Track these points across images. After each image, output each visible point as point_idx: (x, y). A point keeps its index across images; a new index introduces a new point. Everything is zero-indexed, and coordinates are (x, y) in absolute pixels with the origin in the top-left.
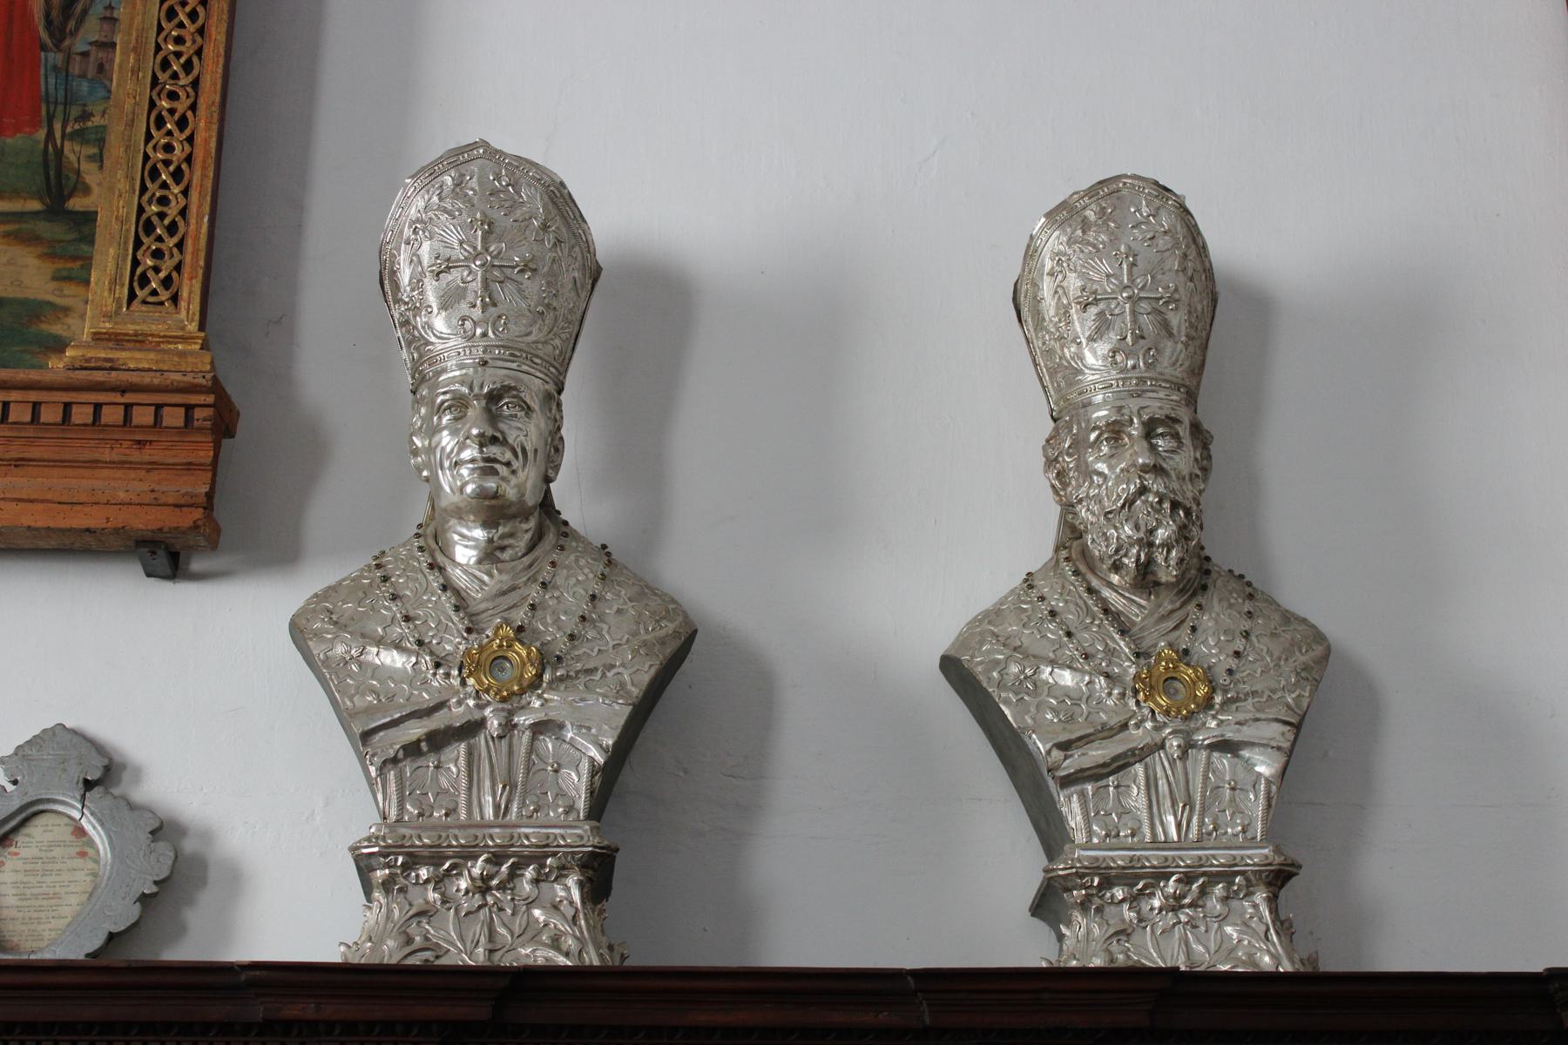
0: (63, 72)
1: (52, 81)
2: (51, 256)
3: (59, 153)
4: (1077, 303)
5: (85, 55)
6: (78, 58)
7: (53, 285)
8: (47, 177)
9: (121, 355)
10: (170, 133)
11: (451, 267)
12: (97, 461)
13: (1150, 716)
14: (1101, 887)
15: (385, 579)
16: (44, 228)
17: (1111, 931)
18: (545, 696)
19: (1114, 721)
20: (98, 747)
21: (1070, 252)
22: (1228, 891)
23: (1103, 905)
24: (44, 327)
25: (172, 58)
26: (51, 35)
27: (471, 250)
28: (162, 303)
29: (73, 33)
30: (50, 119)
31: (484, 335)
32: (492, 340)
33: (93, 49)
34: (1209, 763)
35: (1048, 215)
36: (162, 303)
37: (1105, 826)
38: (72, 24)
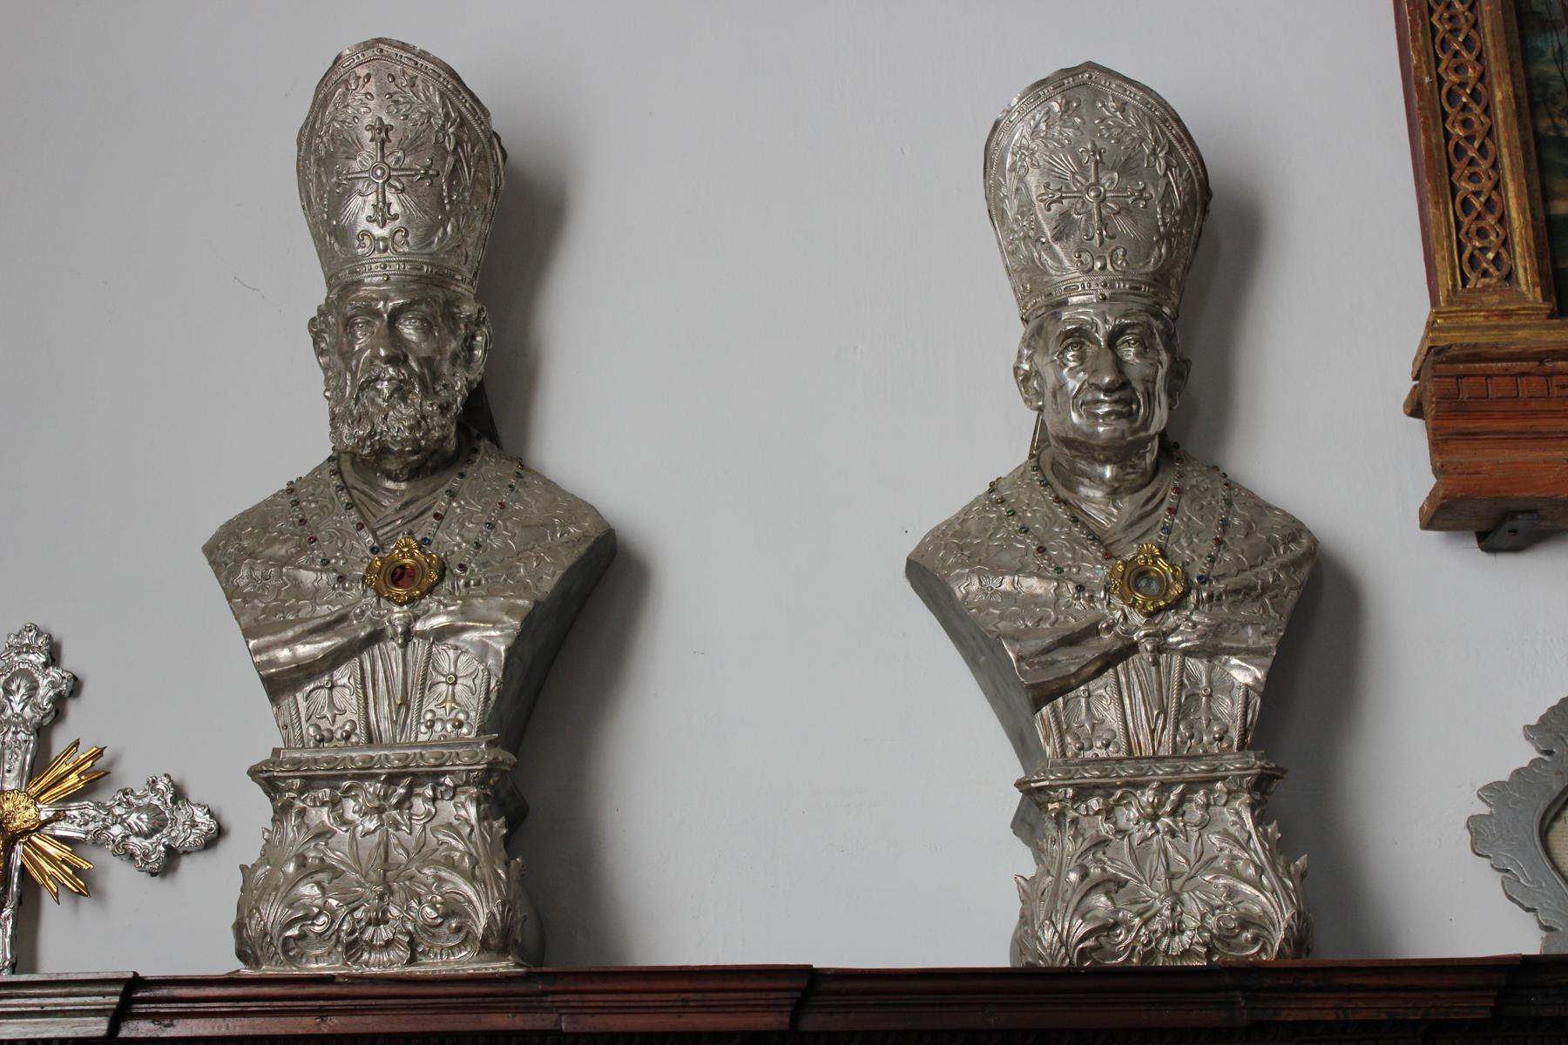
4: (1042, 201)
10: (1465, 107)
11: (1064, 198)
13: (1121, 620)
14: (1075, 799)
15: (296, 503)
17: (1086, 845)
18: (1194, 618)
19: (1084, 623)
21: (1033, 146)
22: (1208, 799)
23: (1077, 818)
27: (1083, 181)
31: (1103, 268)
32: (1111, 274)
34: (1183, 667)
37: (1077, 738)
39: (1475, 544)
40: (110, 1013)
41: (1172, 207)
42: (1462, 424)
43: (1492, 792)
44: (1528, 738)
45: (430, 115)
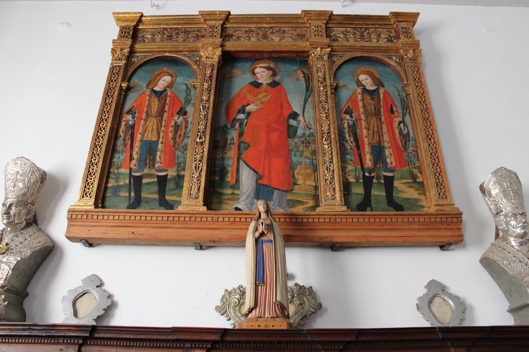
0: (408, 156)
1: (407, 158)
2: (417, 190)
3: (412, 171)
5: (411, 153)
6: (410, 153)
7: (419, 196)
8: (411, 176)
9: (444, 208)
12: (441, 229)
16: (413, 185)
20: (101, 280)
24: (419, 203)
25: (432, 153)
26: (404, 149)
28: (444, 198)
29: (408, 149)
30: (409, 165)
33: (412, 152)
35: (492, 173)
36: (444, 198)
38: (407, 147)
39: (330, 250)
40: (89, 331)
41: (30, 182)
42: (73, 223)
43: (419, 298)
44: (425, 288)
45: (27, 170)
